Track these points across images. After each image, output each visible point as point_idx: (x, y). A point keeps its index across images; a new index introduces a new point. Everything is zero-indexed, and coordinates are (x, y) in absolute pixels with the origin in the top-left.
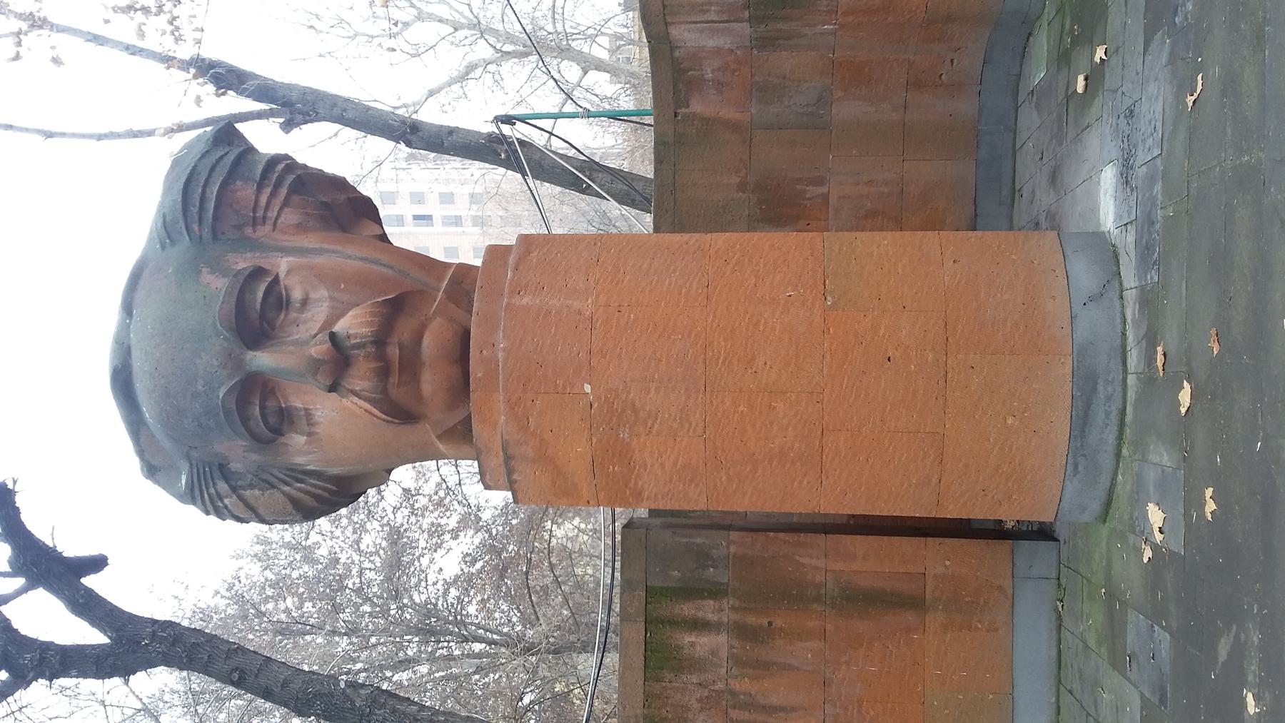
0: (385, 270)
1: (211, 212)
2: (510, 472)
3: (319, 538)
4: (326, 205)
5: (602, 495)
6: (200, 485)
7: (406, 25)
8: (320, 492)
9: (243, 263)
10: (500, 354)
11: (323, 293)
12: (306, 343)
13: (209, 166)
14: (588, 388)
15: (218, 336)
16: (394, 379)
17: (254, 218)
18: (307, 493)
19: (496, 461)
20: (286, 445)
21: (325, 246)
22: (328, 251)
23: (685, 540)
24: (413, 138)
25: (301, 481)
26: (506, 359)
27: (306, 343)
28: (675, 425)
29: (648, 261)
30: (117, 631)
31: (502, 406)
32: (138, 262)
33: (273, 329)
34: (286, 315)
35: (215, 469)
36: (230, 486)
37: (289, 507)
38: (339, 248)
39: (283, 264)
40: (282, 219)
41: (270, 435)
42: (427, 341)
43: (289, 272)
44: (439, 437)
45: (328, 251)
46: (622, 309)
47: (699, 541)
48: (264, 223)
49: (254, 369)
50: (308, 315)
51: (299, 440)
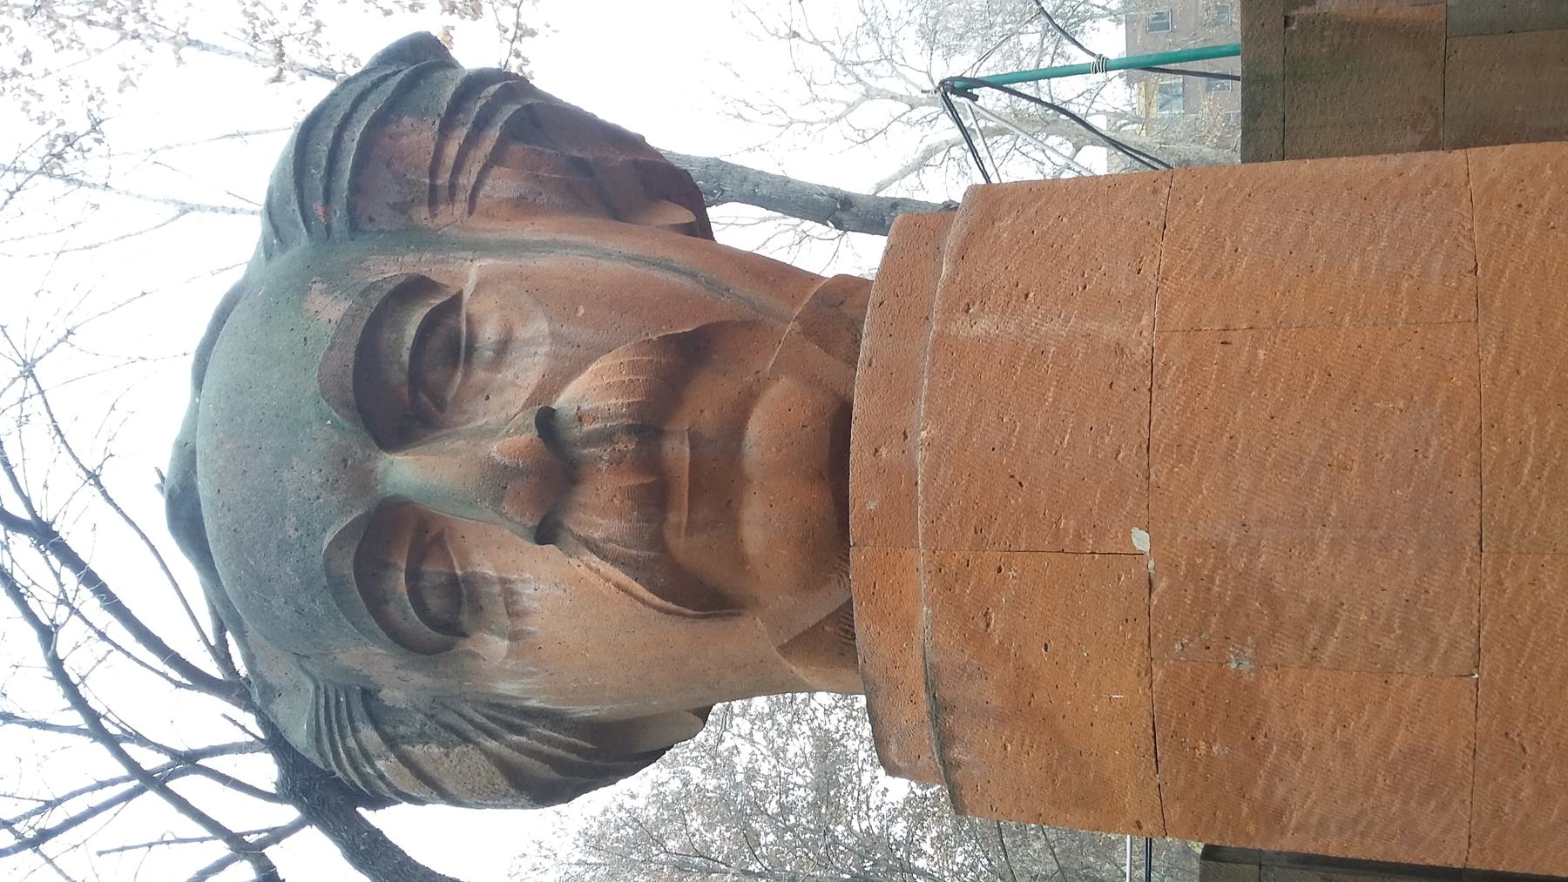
0: (676, 279)
1: (347, 175)
2: (944, 741)
4: (580, 165)
5: (1174, 812)
6: (338, 721)
7: (851, 107)
9: (389, 269)
14: (1141, 540)
15: (323, 419)
16: (678, 516)
17: (433, 188)
18: (533, 753)
19: (912, 713)
20: (474, 656)
21: (565, 237)
22: (566, 245)
24: (844, 216)
25: (519, 730)
26: (933, 468)
28: (1388, 643)
31: (924, 582)
34: (466, 376)
35: (356, 700)
36: (385, 737)
37: (501, 782)
38: (591, 240)
39: (469, 273)
40: (486, 189)
41: (435, 635)
42: (757, 429)
43: (479, 286)
44: (785, 649)
45: (577, 246)
46: (1235, 337)
48: (452, 197)
49: (390, 491)
50: (507, 374)
51: (497, 646)
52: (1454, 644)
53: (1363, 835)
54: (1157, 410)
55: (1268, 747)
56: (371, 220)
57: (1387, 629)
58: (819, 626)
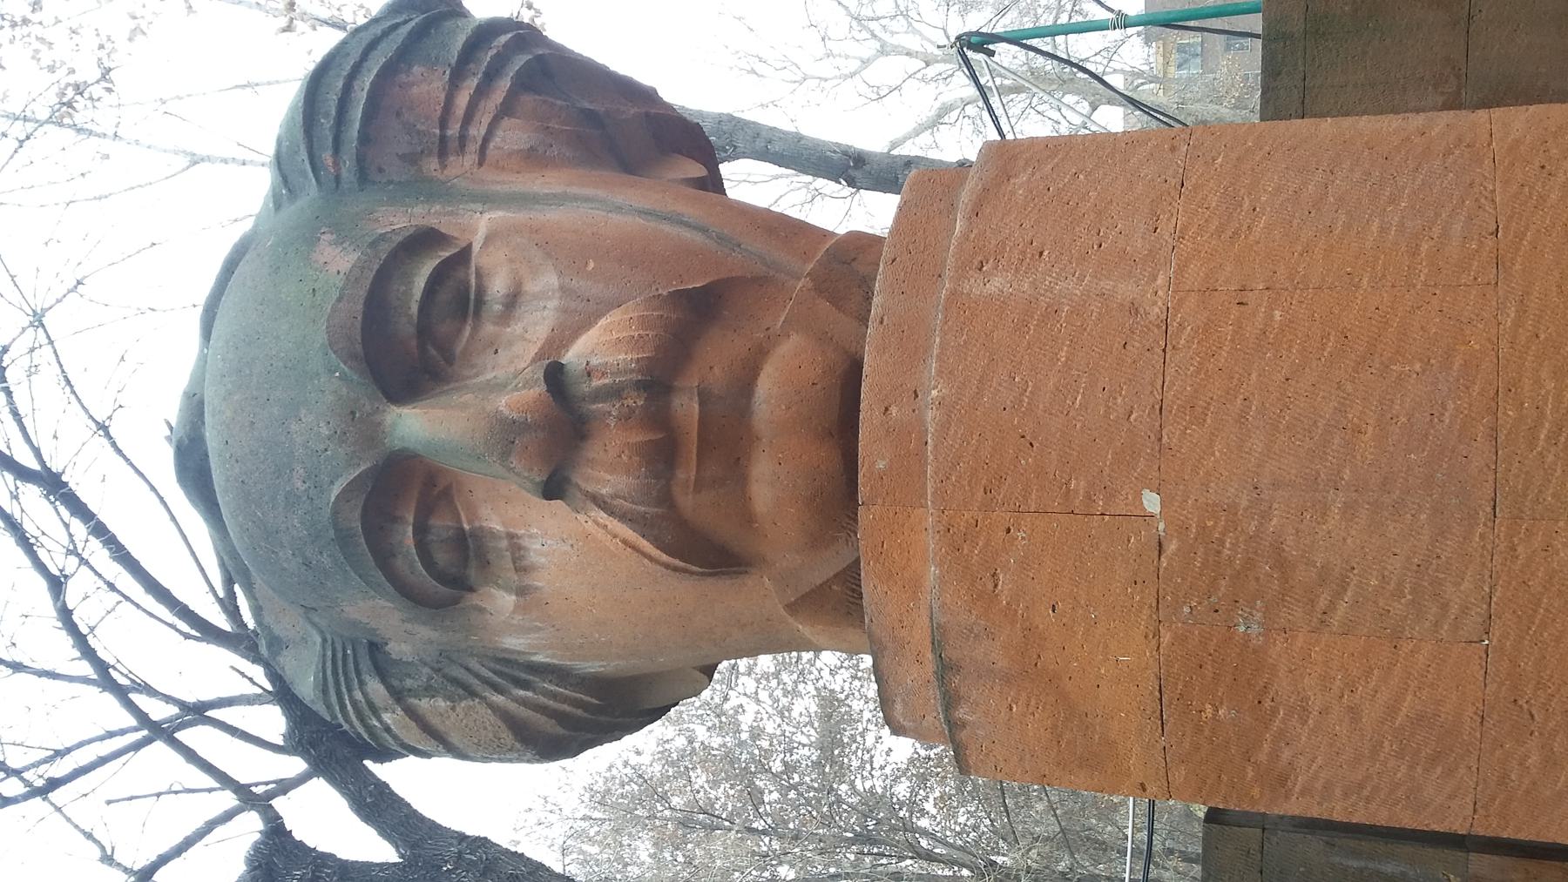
0: (687, 234)
1: (357, 125)
2: (950, 701)
3: (744, 700)
4: (590, 116)
5: (1179, 775)
7: (866, 63)
8: (566, 708)
9: (398, 220)
10: (930, 415)
11: (550, 279)
12: (499, 387)
13: (364, 44)
14: (1152, 502)
16: (686, 473)
17: (443, 139)
19: (917, 674)
20: (482, 610)
22: (576, 198)
23: (1355, 864)
24: (857, 174)
25: (525, 685)
26: (944, 427)
27: (499, 387)
29: (1319, 176)
30: (413, 847)
31: (931, 542)
32: (236, 246)
33: (450, 360)
34: (475, 329)
36: (389, 687)
37: (507, 737)
39: (479, 225)
40: (497, 141)
42: (767, 386)
43: (489, 240)
44: (792, 608)
46: (1250, 297)
47: (1389, 868)
49: (398, 445)
50: (516, 328)
52: (1465, 610)
53: (1368, 800)
54: (1170, 371)
55: (1274, 711)
56: (381, 170)
57: (1398, 594)
58: (827, 584)
